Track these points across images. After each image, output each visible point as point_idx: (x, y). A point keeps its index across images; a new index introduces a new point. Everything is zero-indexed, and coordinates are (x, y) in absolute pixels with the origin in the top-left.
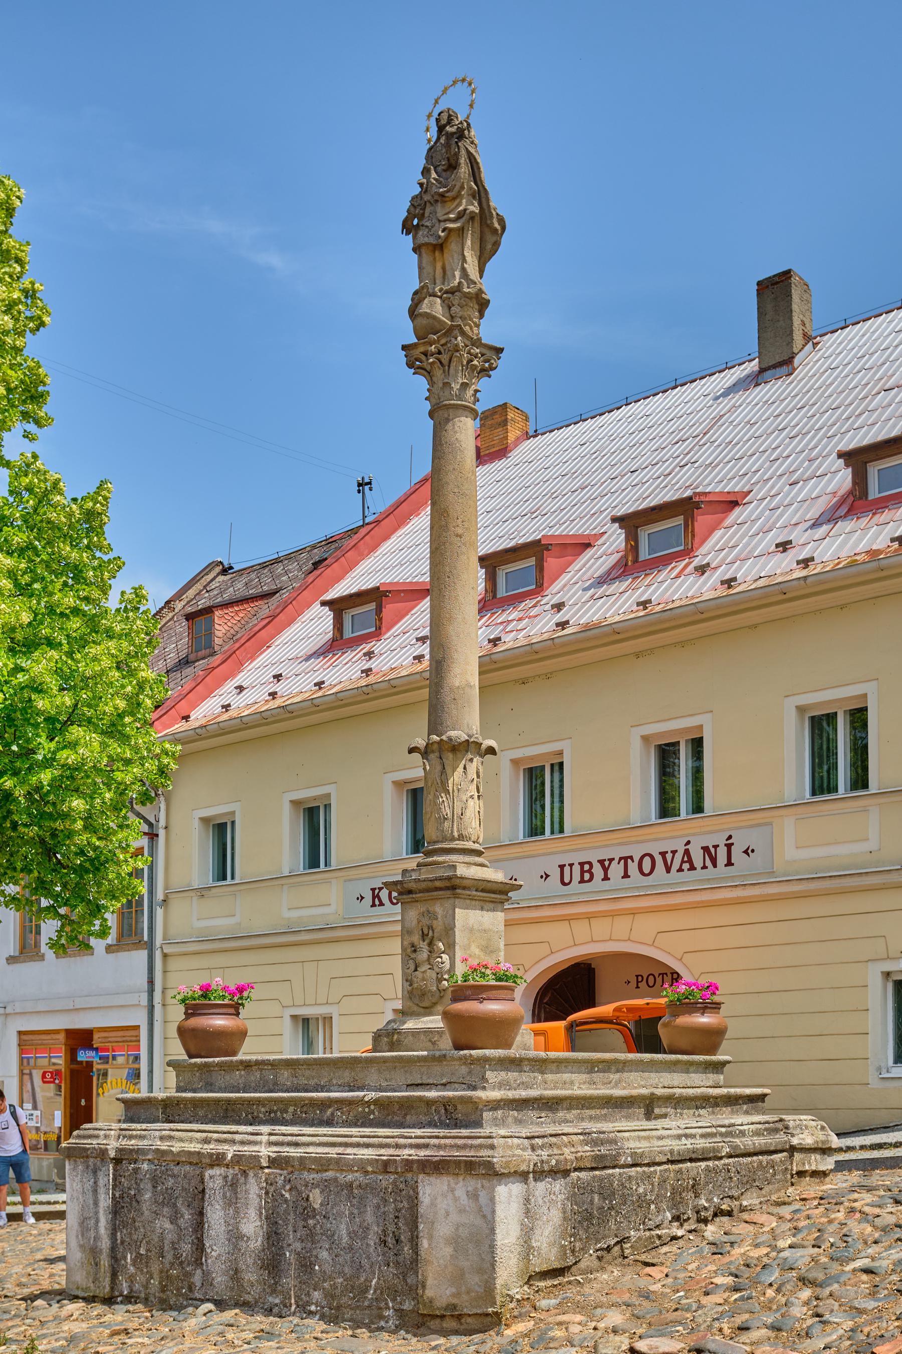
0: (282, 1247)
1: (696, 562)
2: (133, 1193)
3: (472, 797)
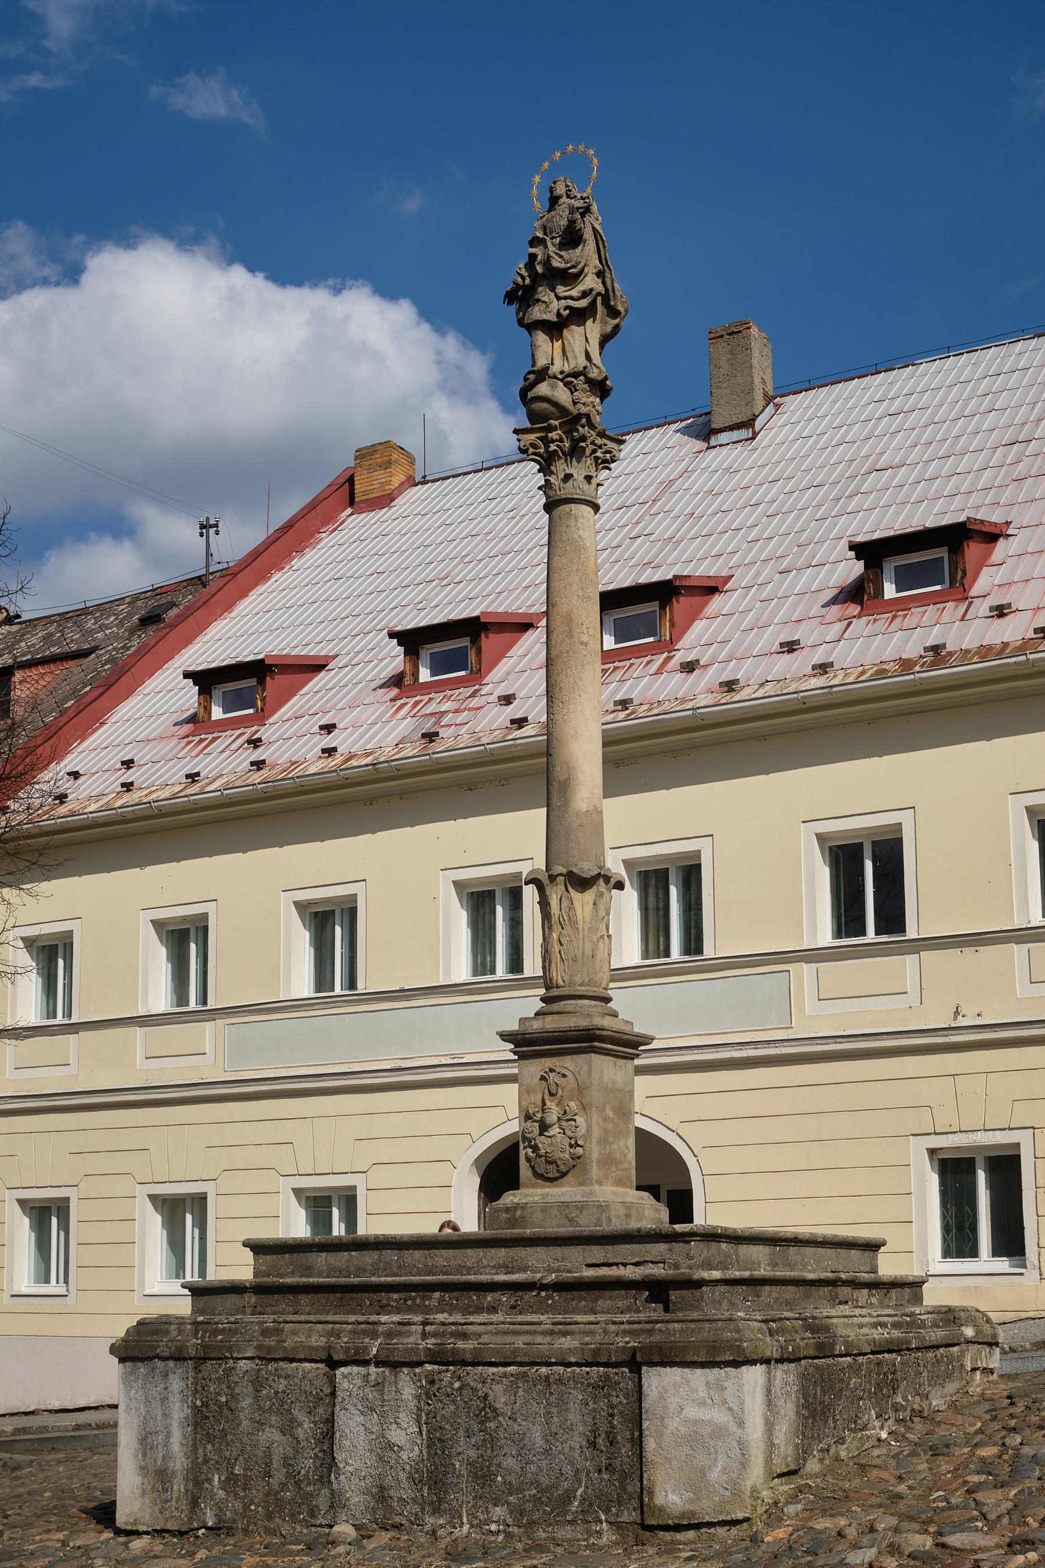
0: (450, 1456)
1: (679, 657)
2: (223, 1399)
3: (602, 936)
